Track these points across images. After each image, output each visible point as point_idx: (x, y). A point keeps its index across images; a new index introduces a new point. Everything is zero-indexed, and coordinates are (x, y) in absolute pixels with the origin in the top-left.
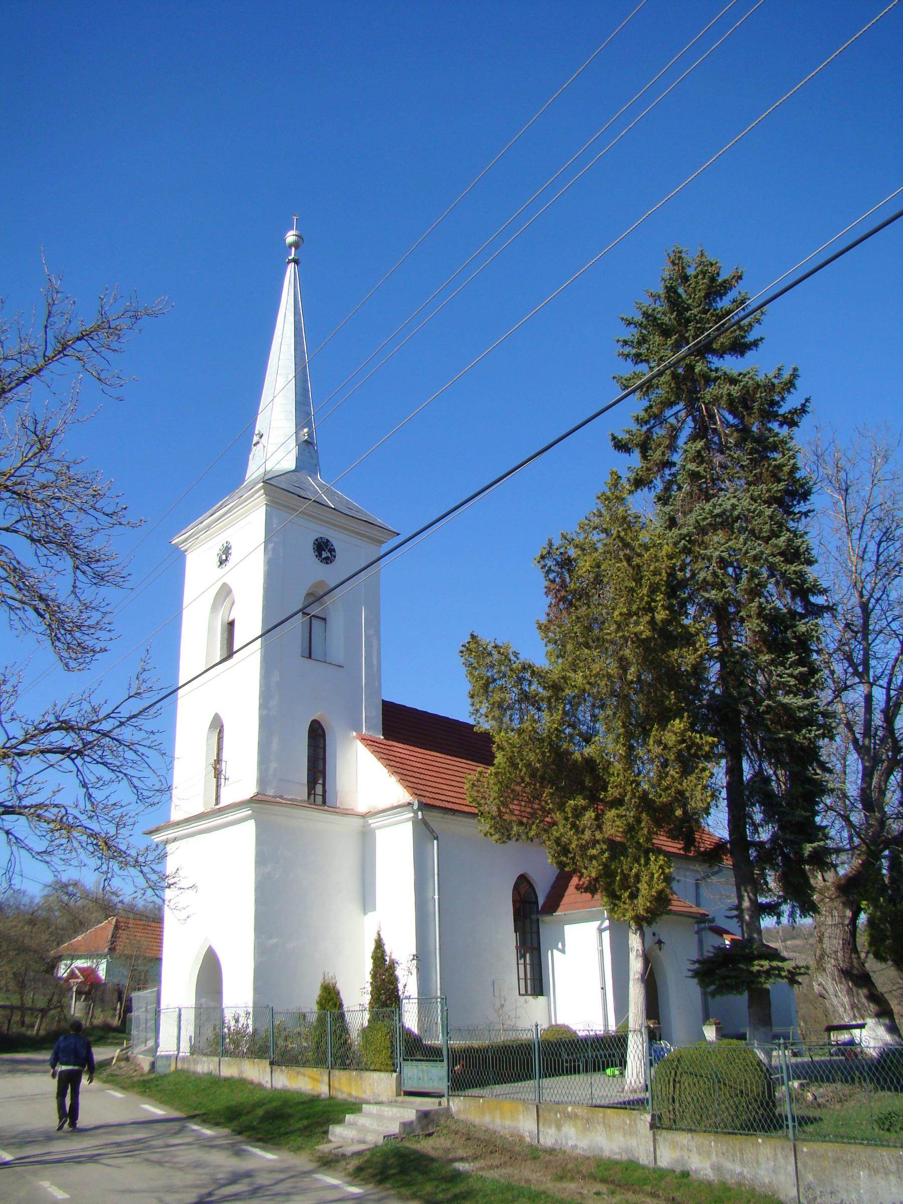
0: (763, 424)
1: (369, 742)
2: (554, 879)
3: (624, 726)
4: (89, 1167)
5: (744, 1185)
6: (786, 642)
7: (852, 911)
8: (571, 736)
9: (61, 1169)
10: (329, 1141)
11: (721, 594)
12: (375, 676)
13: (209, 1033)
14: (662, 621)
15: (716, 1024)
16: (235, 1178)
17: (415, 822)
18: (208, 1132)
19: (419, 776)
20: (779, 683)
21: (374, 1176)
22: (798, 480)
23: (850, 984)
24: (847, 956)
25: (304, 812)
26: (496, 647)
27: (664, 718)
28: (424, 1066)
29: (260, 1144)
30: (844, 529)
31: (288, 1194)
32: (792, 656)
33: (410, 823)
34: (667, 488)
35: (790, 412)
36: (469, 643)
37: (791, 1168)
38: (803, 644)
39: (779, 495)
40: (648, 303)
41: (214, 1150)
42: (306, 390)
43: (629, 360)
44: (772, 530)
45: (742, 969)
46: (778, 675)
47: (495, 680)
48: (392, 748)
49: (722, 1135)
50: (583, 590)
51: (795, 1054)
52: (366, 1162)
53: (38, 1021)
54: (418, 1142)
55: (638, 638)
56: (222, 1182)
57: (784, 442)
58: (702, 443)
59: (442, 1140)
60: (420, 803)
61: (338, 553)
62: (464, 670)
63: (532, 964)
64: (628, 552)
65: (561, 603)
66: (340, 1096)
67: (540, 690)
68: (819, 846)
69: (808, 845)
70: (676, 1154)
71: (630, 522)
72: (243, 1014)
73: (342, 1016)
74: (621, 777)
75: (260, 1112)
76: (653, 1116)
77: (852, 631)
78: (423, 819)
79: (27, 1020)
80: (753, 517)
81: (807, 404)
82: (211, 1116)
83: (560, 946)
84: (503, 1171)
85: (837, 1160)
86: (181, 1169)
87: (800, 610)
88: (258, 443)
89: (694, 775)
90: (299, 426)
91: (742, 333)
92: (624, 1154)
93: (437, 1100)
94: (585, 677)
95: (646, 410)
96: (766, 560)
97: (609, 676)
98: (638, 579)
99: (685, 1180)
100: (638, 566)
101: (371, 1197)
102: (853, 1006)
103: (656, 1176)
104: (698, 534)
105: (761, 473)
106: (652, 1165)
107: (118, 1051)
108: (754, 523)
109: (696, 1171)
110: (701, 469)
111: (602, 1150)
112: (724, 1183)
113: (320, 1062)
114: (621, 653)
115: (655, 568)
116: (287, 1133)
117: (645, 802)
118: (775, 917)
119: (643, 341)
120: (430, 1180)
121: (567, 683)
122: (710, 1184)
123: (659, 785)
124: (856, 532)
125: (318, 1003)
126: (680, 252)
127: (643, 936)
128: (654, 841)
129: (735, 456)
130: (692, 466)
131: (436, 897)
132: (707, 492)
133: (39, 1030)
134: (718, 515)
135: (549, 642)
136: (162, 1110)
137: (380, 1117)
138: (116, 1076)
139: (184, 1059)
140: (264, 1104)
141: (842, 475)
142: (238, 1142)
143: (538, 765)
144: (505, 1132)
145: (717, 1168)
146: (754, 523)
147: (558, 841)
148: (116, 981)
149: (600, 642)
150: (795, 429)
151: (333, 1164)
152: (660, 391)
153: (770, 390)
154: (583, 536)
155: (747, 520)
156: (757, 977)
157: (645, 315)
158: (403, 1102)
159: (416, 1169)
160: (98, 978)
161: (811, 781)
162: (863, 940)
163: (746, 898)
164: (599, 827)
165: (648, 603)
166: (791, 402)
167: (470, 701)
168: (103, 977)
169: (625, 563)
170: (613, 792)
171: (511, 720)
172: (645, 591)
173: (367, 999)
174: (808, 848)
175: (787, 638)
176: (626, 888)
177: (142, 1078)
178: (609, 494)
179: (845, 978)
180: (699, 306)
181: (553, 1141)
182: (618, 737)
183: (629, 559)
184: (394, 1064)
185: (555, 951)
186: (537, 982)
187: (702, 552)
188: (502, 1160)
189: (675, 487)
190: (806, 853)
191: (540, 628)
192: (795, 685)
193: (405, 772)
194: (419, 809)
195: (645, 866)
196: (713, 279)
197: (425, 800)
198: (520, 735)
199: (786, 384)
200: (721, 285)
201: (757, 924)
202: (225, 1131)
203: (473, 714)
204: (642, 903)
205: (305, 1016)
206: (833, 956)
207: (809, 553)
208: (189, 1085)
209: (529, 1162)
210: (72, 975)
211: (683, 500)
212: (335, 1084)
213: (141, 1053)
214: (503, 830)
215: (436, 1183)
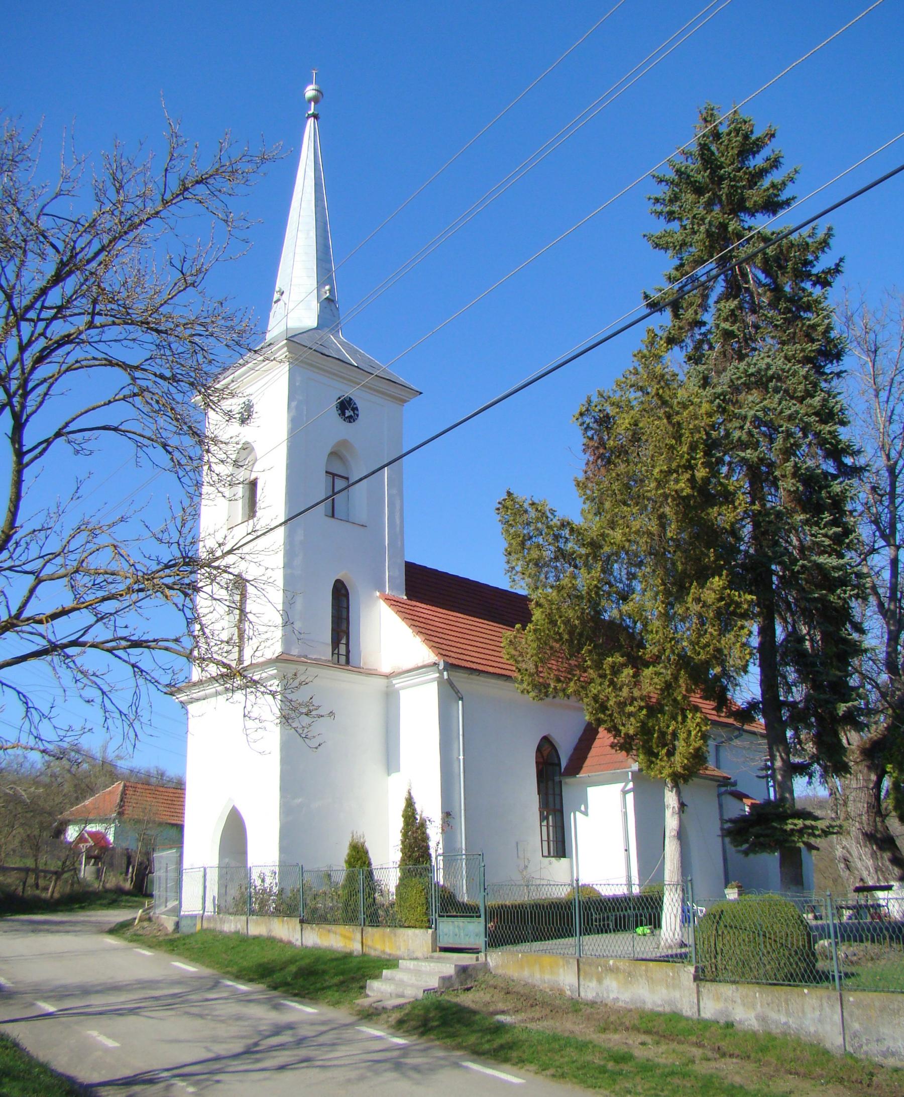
0: (796, 284)
1: (392, 602)
2: (577, 740)
3: (664, 584)
4: (132, 1019)
5: (790, 1034)
6: (821, 502)
7: (877, 775)
8: (609, 594)
9: (104, 1020)
10: (367, 996)
11: (756, 454)
12: (398, 537)
13: (234, 892)
14: (702, 479)
15: (738, 887)
16: (278, 1030)
17: (441, 682)
18: (243, 987)
19: (443, 636)
20: (814, 543)
21: (416, 1028)
22: (833, 340)
23: (875, 848)
24: (872, 819)
25: (331, 672)
26: (533, 504)
27: (702, 576)
28: (460, 922)
29: (296, 998)
30: (872, 392)
31: (334, 1044)
32: (827, 517)
33: (436, 683)
34: (698, 346)
35: (823, 272)
36: (504, 500)
37: (837, 1017)
38: (837, 504)
39: (813, 355)
40: (682, 162)
41: (251, 1005)
42: (327, 247)
43: (662, 218)
44: (806, 391)
45: (776, 828)
46: (812, 535)
47: (530, 538)
48: (415, 609)
49: (768, 987)
50: (622, 447)
51: (816, 918)
52: (407, 1014)
53: (53, 883)
54: (457, 996)
55: (679, 496)
56: (267, 1033)
57: (818, 302)
58: (736, 302)
59: (481, 994)
60: (446, 663)
61: (361, 412)
62: (500, 527)
63: (555, 826)
64: (667, 409)
65: (599, 461)
66: (373, 953)
67: (576, 547)
68: (853, 706)
69: (843, 705)
70: (720, 1006)
71: (667, 380)
72: (268, 874)
73: (371, 874)
74: (661, 634)
75: (293, 968)
76: (697, 968)
77: (879, 495)
78: (449, 680)
79: (42, 883)
80: (787, 377)
81: (841, 264)
82: (244, 973)
83: (583, 808)
84: (545, 1023)
85: (883, 1010)
86: (222, 1021)
87: (832, 471)
88: (278, 300)
89: (733, 633)
90: (320, 285)
91: (775, 192)
92: (666, 1006)
93: (475, 956)
94: (624, 534)
95: (677, 269)
96: (801, 420)
97: (650, 534)
98: (678, 437)
99: (731, 1031)
100: (679, 423)
101: (417, 1047)
102: (877, 869)
103: (700, 1026)
104: (732, 394)
105: (795, 333)
106: (696, 1016)
107: (141, 911)
108: (788, 382)
109: (740, 1022)
110: (735, 328)
111: (644, 1002)
112: (769, 1033)
113: (350, 918)
114: (662, 510)
115: (695, 426)
116: (323, 989)
117: (684, 661)
118: (807, 778)
119: (675, 199)
120: (474, 1032)
121: (604, 540)
122: (755, 1034)
123: (698, 643)
124: (883, 395)
125: (346, 862)
126: (712, 109)
127: (679, 793)
128: (691, 699)
129: (769, 315)
130: (726, 325)
131: (461, 757)
132: (740, 351)
133: (53, 892)
134: (752, 374)
135: (587, 499)
136: (194, 967)
137: (418, 972)
138: (141, 935)
139: (209, 919)
140: (296, 961)
141: (871, 336)
142: (275, 997)
143: (577, 622)
144: (545, 986)
145: (763, 1019)
146: (788, 382)
147: (595, 698)
148: (125, 845)
149: (639, 499)
150: (706, 314)
151: (375, 1018)
152: (693, 249)
153: (804, 249)
154: (619, 393)
155: (779, 379)
156: (790, 835)
157: (679, 172)
158: (439, 958)
159: (459, 1022)
160: (107, 842)
161: (845, 641)
162: (888, 804)
163: (778, 758)
164: (637, 684)
165: (688, 461)
166: (825, 262)
167: (505, 559)
168: (112, 841)
169: (665, 421)
170: (651, 650)
171: (546, 578)
172: (685, 448)
173: (399, 856)
174: (842, 708)
175: (822, 498)
176: (664, 745)
177: (167, 938)
178: (645, 351)
179: (869, 841)
180: (733, 163)
181: (594, 994)
182: (657, 594)
183: (669, 417)
184: (429, 921)
185: (578, 813)
186: (560, 844)
187: (736, 411)
188: (544, 1013)
189: (706, 347)
190: (841, 713)
191: (578, 485)
192: (829, 546)
193: (430, 632)
194: (445, 669)
195: (682, 724)
196: (746, 137)
197: (451, 661)
198: (559, 591)
199: (820, 243)
200: (754, 143)
201: (789, 783)
202: (261, 987)
203: (508, 571)
204: (679, 761)
205: (329, 876)
206: (858, 819)
207: (843, 414)
208: (217, 943)
209: (570, 1015)
210: (81, 839)
211: (716, 359)
212: (368, 941)
213: (163, 913)
214: (542, 689)
215: (480, 1034)
